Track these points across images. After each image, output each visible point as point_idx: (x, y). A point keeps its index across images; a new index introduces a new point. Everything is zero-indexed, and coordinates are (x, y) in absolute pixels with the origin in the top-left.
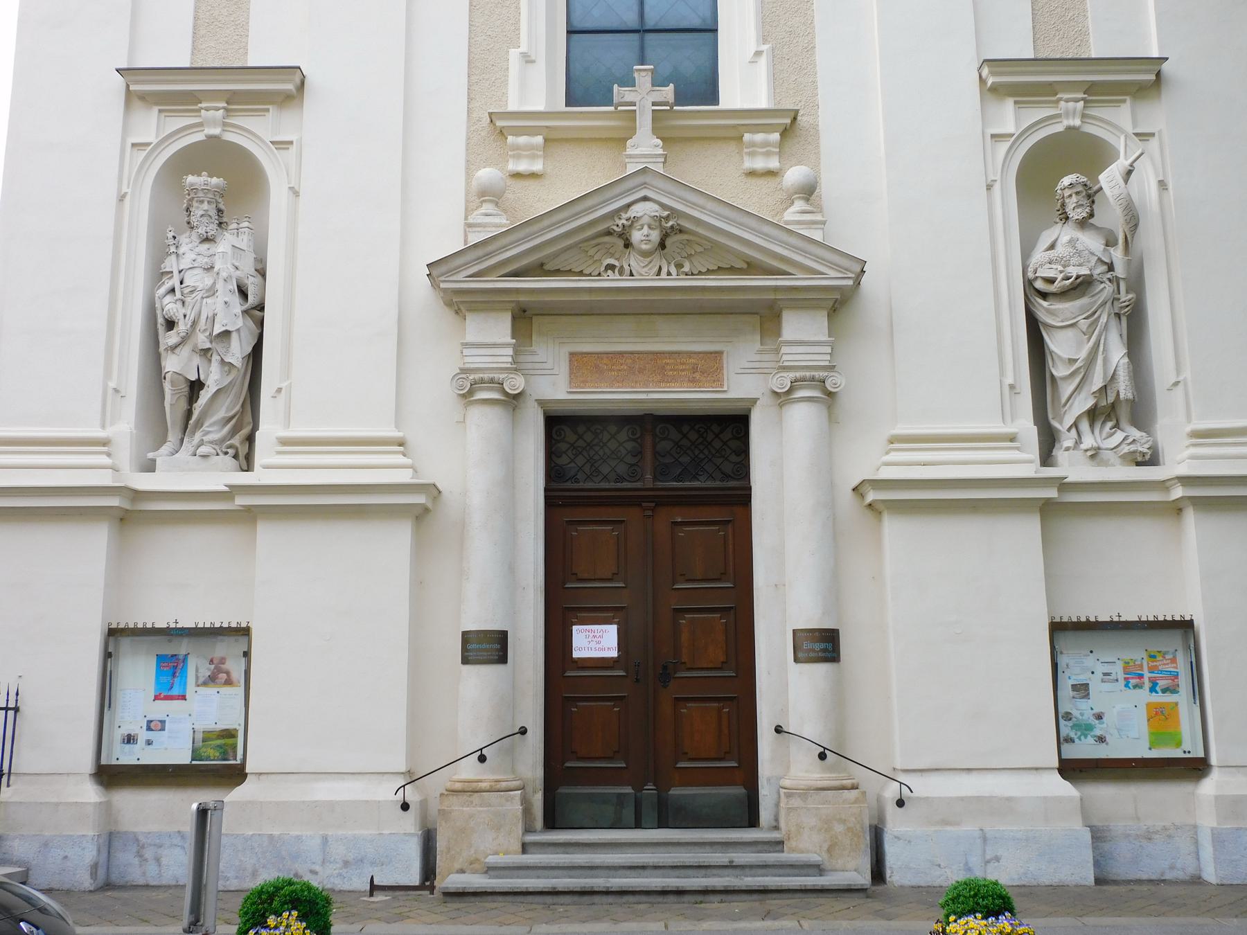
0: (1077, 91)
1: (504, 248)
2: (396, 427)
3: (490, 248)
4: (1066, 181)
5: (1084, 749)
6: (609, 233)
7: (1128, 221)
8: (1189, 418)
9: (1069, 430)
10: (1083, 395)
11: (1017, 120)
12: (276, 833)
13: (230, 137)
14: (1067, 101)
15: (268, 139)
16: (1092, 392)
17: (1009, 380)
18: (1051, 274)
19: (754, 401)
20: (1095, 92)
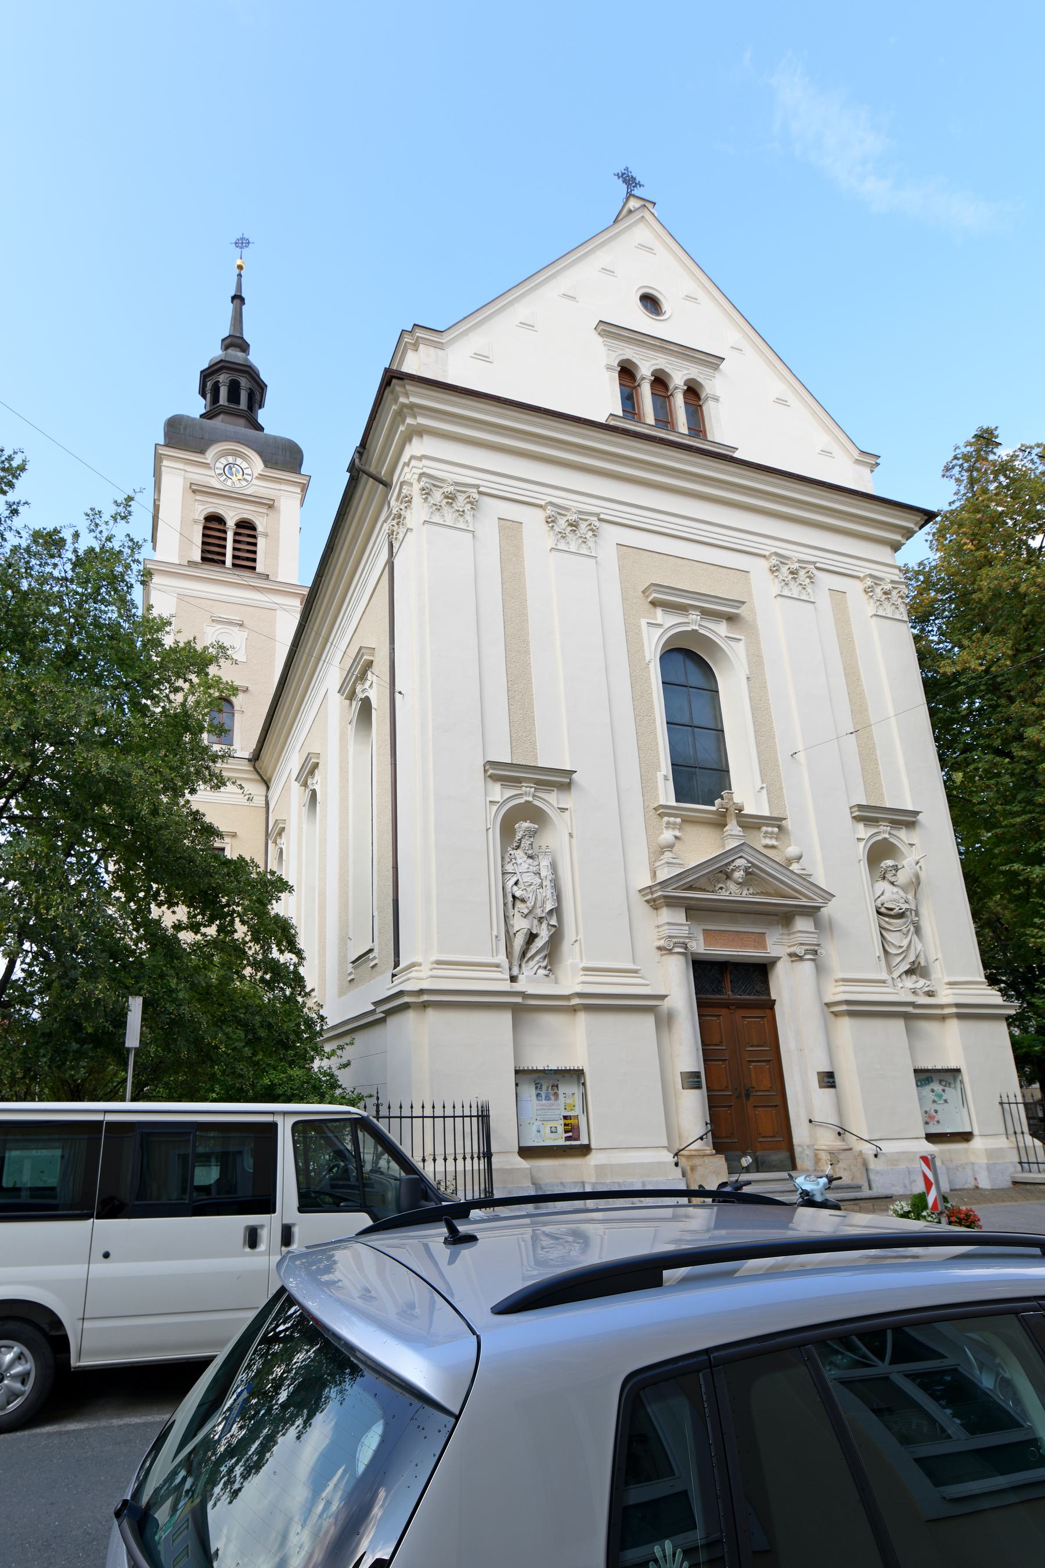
0: (530, 783)
1: (687, 877)
2: (634, 963)
3: (683, 876)
5: (934, 1129)
6: (721, 872)
8: (582, 961)
10: (904, 963)
11: (866, 833)
12: (621, 1181)
13: (536, 803)
14: (526, 787)
15: (907, 842)
17: (878, 954)
19: (779, 958)
20: (896, 824)
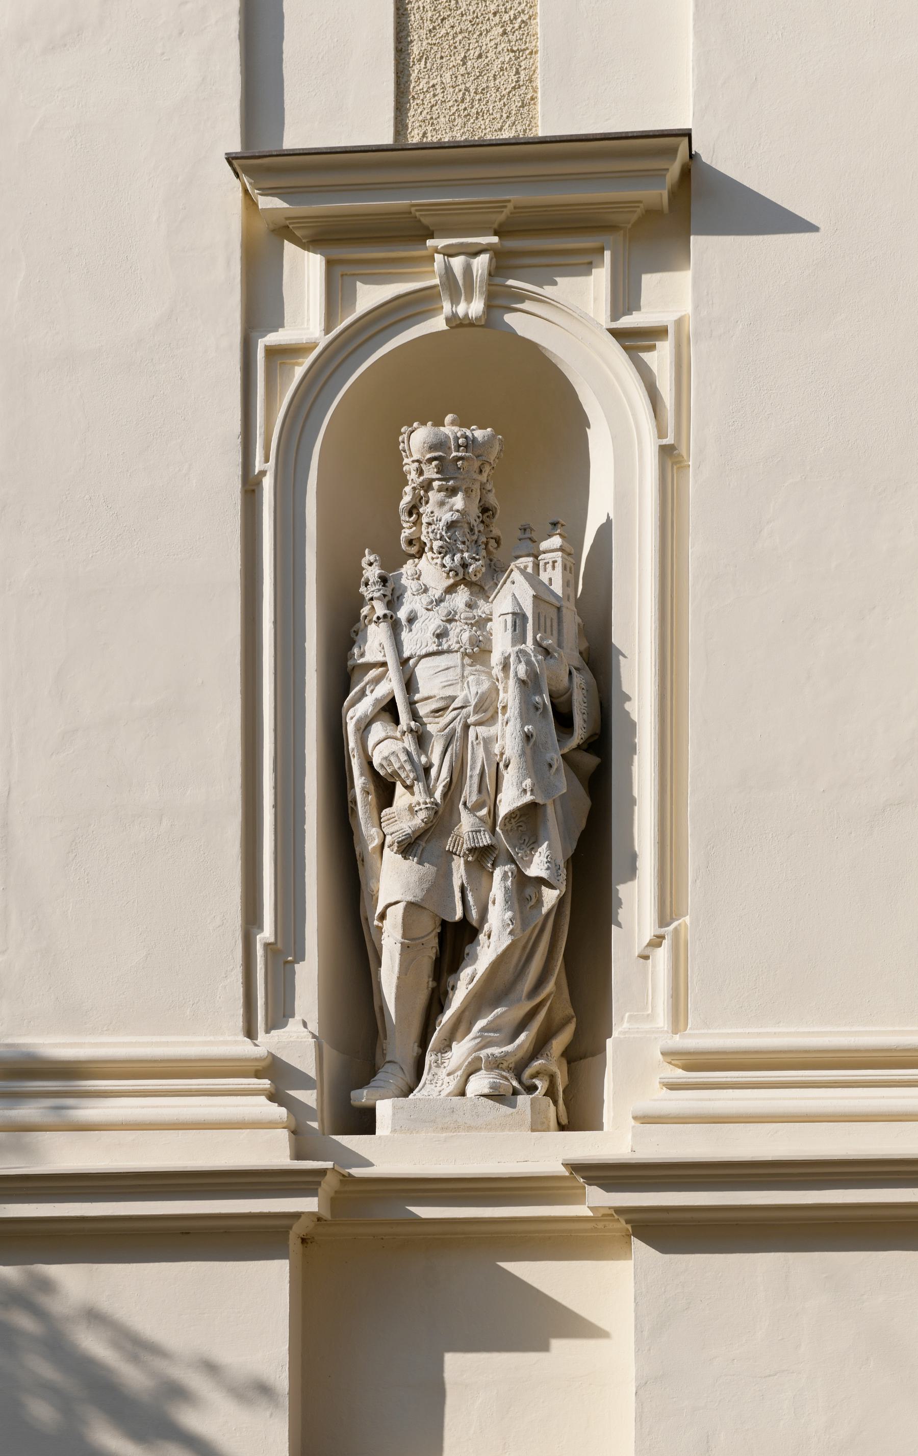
14: (449, 253)
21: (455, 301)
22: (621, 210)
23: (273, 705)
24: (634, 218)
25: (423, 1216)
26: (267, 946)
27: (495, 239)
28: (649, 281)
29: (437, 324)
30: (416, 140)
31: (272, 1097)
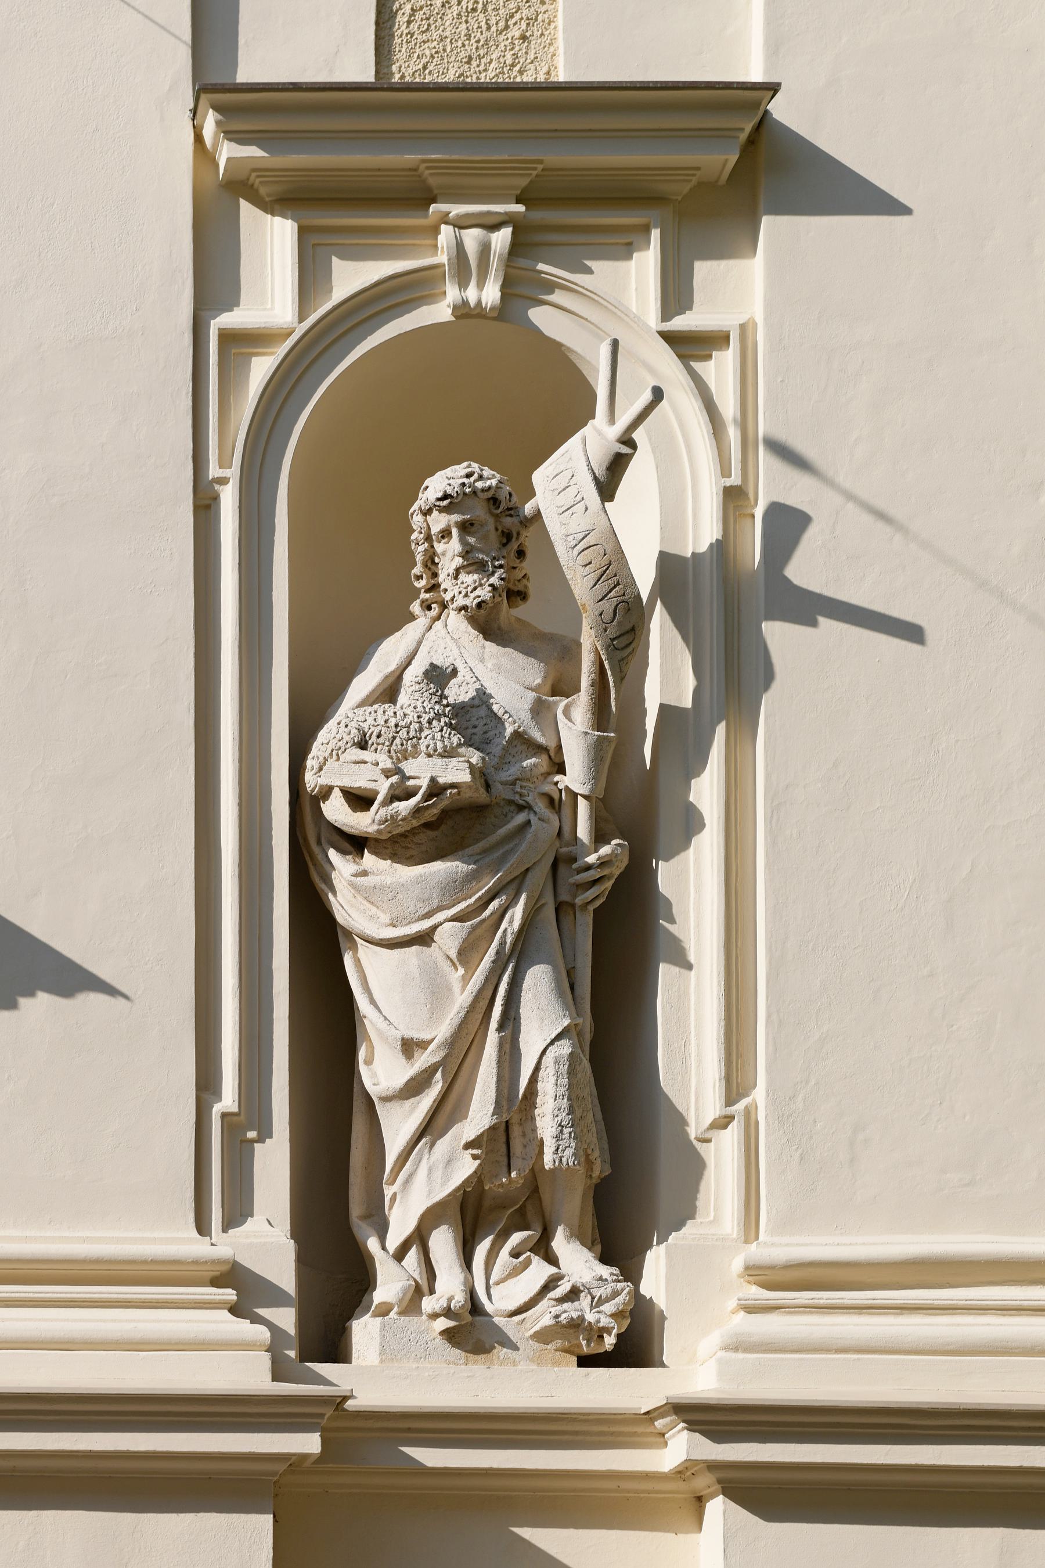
4: (436, 485)
7: (608, 616)
9: (400, 1255)
10: (443, 1145)
14: (461, 224)
16: (463, 1142)
18: (360, 780)
21: (463, 284)
22: (668, 178)
23: (237, 950)
24: (686, 188)
25: (430, 1463)
26: (224, 1116)
27: (520, 208)
28: (703, 270)
29: (440, 312)
30: (396, 78)
31: (235, 1310)
